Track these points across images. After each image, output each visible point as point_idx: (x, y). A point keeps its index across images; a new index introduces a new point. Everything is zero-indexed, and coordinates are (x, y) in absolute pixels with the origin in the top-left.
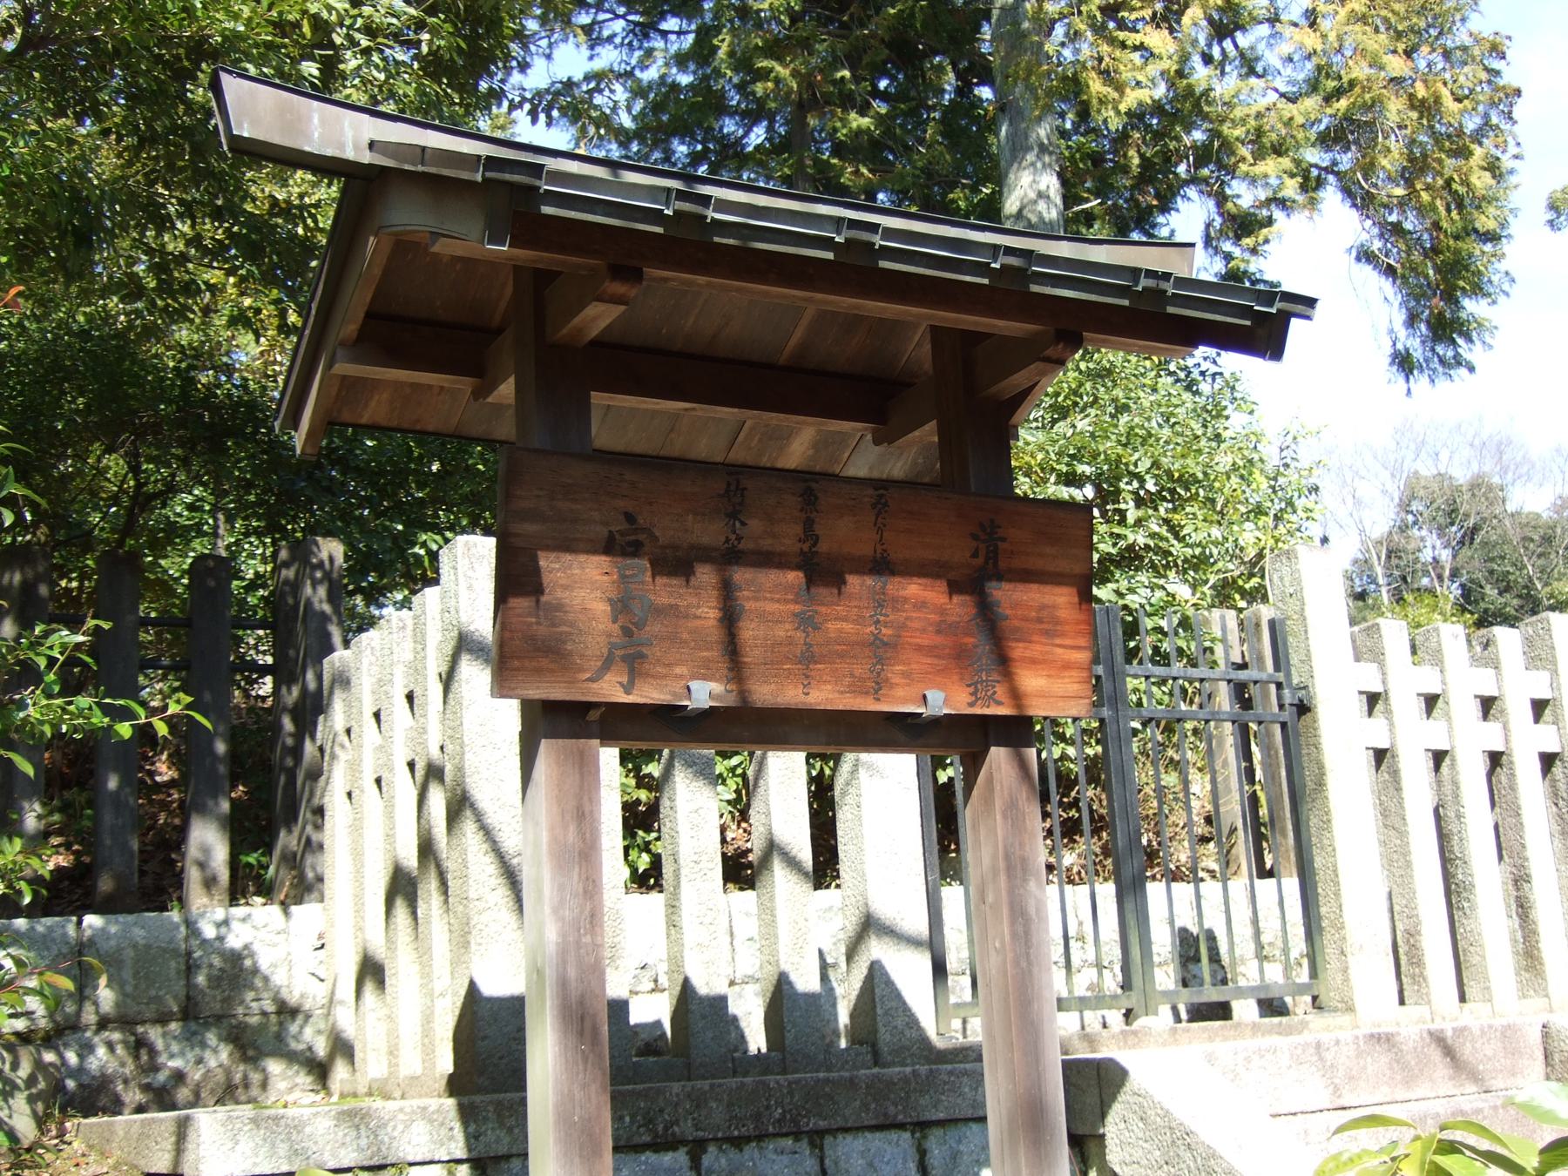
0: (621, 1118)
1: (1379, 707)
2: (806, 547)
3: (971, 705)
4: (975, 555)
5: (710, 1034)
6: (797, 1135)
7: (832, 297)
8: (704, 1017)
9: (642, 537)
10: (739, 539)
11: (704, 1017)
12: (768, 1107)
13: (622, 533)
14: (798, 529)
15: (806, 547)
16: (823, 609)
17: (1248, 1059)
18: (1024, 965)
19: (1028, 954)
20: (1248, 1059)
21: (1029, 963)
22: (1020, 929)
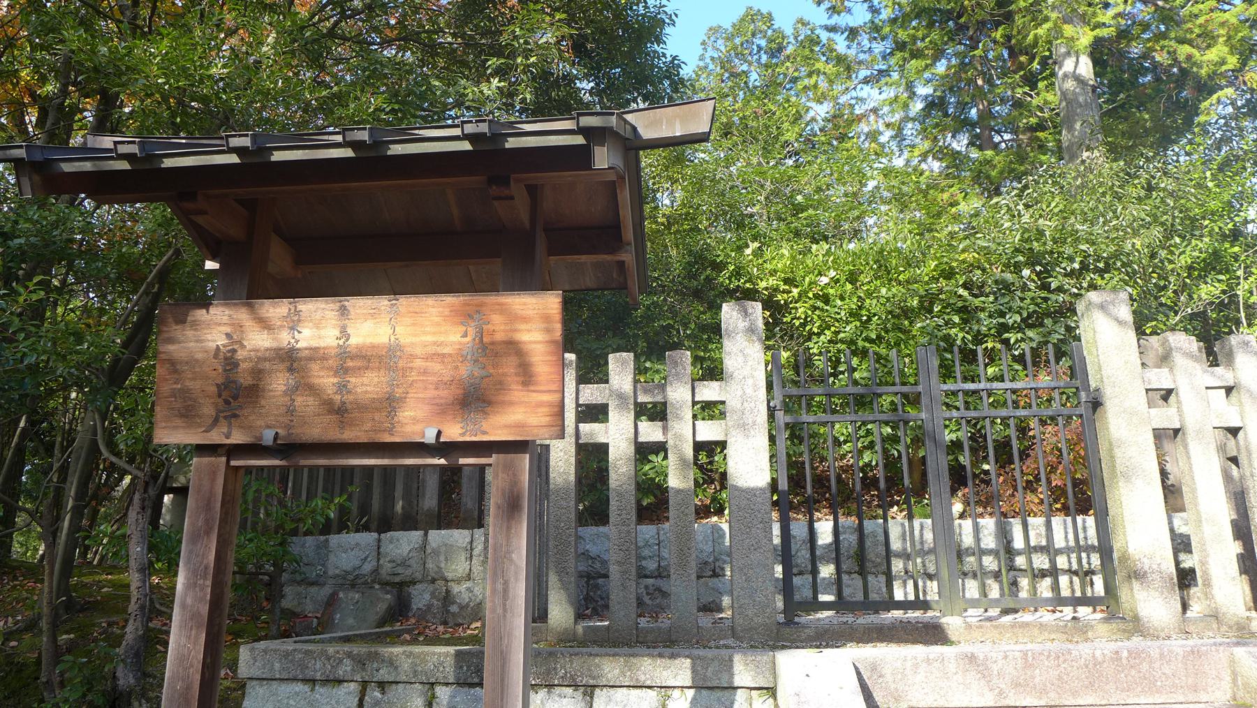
0: (461, 667)
1: (1172, 398)
2: (341, 342)
3: (463, 434)
4: (465, 335)
5: (622, 613)
6: (576, 686)
7: (325, 186)
8: (619, 603)
9: (235, 347)
10: (297, 342)
11: (619, 603)
12: (555, 669)
13: (224, 346)
14: (337, 333)
15: (341, 342)
16: (353, 380)
17: (916, 666)
18: (500, 611)
19: (505, 605)
20: (916, 666)
21: (505, 610)
22: (500, 587)
